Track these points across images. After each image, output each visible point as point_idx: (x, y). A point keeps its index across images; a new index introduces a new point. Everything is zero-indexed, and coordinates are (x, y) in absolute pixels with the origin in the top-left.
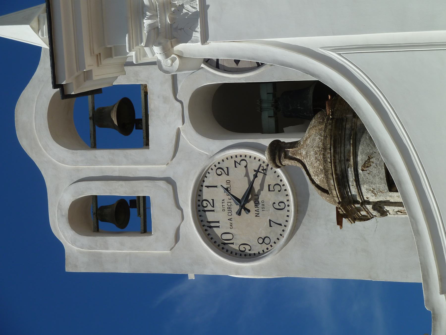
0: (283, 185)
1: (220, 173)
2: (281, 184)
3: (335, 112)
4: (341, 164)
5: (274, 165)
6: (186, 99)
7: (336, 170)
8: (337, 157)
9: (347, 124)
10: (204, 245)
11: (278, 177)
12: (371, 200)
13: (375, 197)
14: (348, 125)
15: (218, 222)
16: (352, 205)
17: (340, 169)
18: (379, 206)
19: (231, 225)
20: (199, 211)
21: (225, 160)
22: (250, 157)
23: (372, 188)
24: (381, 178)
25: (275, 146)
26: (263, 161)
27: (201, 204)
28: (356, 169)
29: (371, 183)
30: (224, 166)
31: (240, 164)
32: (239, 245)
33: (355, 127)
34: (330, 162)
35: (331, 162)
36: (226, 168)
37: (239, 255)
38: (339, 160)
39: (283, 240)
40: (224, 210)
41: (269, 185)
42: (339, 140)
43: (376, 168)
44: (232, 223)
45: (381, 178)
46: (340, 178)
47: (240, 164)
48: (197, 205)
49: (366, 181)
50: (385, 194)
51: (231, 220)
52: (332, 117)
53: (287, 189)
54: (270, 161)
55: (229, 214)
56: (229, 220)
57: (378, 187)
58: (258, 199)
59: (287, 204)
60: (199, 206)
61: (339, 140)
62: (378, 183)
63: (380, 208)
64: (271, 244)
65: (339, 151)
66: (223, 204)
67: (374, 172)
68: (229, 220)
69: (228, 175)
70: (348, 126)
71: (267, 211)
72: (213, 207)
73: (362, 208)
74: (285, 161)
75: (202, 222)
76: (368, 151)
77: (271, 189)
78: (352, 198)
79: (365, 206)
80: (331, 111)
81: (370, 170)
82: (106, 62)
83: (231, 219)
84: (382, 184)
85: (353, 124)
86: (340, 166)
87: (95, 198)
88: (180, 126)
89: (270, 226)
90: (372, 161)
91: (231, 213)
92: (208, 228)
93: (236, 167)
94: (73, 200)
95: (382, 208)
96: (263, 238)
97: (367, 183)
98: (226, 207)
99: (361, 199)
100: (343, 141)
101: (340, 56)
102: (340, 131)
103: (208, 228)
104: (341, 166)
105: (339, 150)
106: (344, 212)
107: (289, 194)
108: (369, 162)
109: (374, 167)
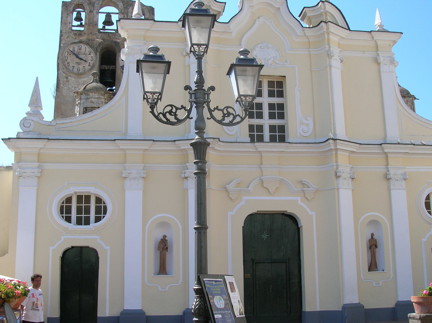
11: (282, 139)
24: (87, 105)
41: (85, 67)
45: (87, 105)
70: (102, 97)
77: (84, 67)
89: (73, 66)
92: (73, 47)
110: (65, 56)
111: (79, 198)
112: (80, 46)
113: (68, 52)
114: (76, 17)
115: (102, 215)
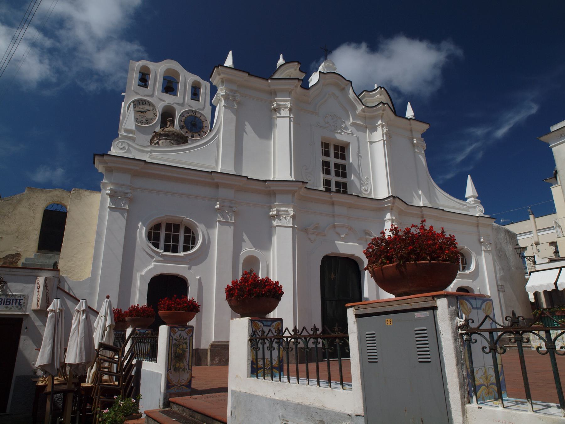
6: (175, 106)
8: (174, 135)
11: (345, 192)
15: (139, 104)
30: (154, 110)
70: (181, 140)
82: (220, 80)
87: (149, 75)
88: (167, 102)
111: (169, 226)
115: (153, 231)
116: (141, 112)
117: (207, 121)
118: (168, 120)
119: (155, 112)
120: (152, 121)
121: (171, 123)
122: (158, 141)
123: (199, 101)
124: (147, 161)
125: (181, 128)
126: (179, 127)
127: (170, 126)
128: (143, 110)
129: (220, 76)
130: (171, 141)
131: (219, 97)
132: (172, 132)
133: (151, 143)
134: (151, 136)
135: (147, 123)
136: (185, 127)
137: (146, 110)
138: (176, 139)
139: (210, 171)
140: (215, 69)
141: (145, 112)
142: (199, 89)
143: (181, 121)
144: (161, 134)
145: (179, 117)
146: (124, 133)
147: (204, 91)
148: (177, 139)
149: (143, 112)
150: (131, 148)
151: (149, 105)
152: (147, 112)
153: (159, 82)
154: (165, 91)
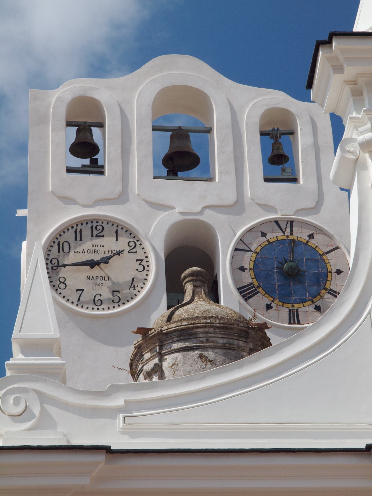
0: (119, 306)
1: (130, 245)
2: (120, 303)
3: (255, 331)
4: (204, 333)
5: (186, 275)
7: (197, 327)
8: (211, 329)
9: (243, 342)
10: (57, 225)
12: (163, 363)
13: (168, 366)
14: (242, 343)
15: (81, 240)
16: (158, 344)
17: (198, 332)
18: (158, 370)
19: (78, 252)
20: (92, 222)
21: (144, 251)
22: (147, 275)
23: (178, 364)
25: (206, 277)
26: (143, 287)
27: (98, 224)
28: (199, 347)
29: (184, 363)
30: (138, 249)
31: (140, 264)
32: (58, 258)
33: (241, 350)
34: (206, 322)
35: (206, 323)
36: (136, 251)
37: (48, 258)
38: (208, 331)
39: (63, 301)
40: (93, 246)
41: (118, 292)
42: (228, 332)
43: (201, 367)
44: (80, 253)
46: (189, 332)
47: (140, 264)
48: (98, 221)
49: (186, 358)
50: (172, 376)
51: (83, 252)
52: (251, 327)
53: (115, 309)
54: (190, 271)
55: (89, 250)
56: (83, 250)
57: (179, 369)
58: (105, 280)
59: (100, 307)
60: (97, 222)
61: (228, 333)
62: (184, 369)
63: (156, 371)
64: (59, 289)
65: (217, 332)
66: (99, 246)
67: (196, 366)
68: (83, 250)
69: (129, 252)
70: (241, 343)
71: (93, 288)
72: (96, 236)
73: (155, 353)
74: (191, 285)
75: (81, 224)
76: (218, 361)
77: (115, 294)
78: (166, 344)
79: (157, 357)
80: (256, 328)
81: (198, 361)
82: (347, 89)
83: (84, 252)
84: (183, 373)
85: (244, 348)
86: (202, 332)
87: (292, 133)
88: (177, 210)
89: (77, 290)
90: (208, 363)
91: (90, 253)
92: (74, 229)
93: (137, 260)
94: (102, 102)
95: (155, 373)
96: (64, 282)
97: (184, 358)
98: (97, 248)
99: (164, 353)
100: (227, 337)
101: (368, 313)
102: (237, 334)
103: (75, 229)
104: (201, 333)
105: (218, 332)
106: (150, 336)
107: (110, 310)
108: (207, 361)
109: (202, 366)
110: (50, 259)
112: (99, 228)
113: (59, 244)
114: (75, 141)
116: (92, 264)
117: (337, 248)
118: (185, 277)
119: (140, 255)
120: (135, 292)
121: (198, 283)
122: (156, 360)
123: (295, 180)
124: (113, 448)
125: (243, 296)
126: (236, 293)
127: (196, 298)
128: (96, 257)
129: (343, 73)
130: (205, 353)
131: (352, 153)
132: (205, 318)
133: (135, 374)
134: (131, 349)
135: (119, 302)
136: (260, 289)
137: (107, 255)
138: (221, 341)
139: (364, 446)
140: (320, 53)
141: (106, 260)
142: (291, 137)
143: (242, 269)
144: (166, 334)
145: (232, 257)
146: (21, 356)
147: (310, 140)
148: (225, 341)
149: (98, 263)
150: (53, 410)
151: (117, 232)
152: (110, 261)
153: (139, 143)
154: (164, 171)
